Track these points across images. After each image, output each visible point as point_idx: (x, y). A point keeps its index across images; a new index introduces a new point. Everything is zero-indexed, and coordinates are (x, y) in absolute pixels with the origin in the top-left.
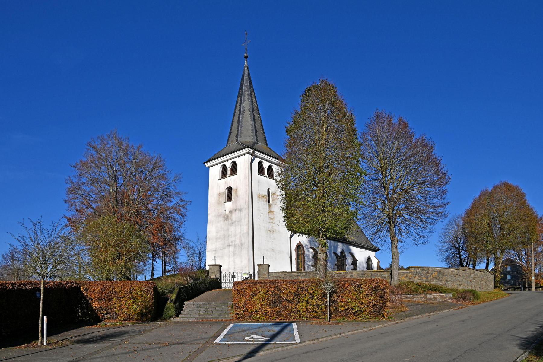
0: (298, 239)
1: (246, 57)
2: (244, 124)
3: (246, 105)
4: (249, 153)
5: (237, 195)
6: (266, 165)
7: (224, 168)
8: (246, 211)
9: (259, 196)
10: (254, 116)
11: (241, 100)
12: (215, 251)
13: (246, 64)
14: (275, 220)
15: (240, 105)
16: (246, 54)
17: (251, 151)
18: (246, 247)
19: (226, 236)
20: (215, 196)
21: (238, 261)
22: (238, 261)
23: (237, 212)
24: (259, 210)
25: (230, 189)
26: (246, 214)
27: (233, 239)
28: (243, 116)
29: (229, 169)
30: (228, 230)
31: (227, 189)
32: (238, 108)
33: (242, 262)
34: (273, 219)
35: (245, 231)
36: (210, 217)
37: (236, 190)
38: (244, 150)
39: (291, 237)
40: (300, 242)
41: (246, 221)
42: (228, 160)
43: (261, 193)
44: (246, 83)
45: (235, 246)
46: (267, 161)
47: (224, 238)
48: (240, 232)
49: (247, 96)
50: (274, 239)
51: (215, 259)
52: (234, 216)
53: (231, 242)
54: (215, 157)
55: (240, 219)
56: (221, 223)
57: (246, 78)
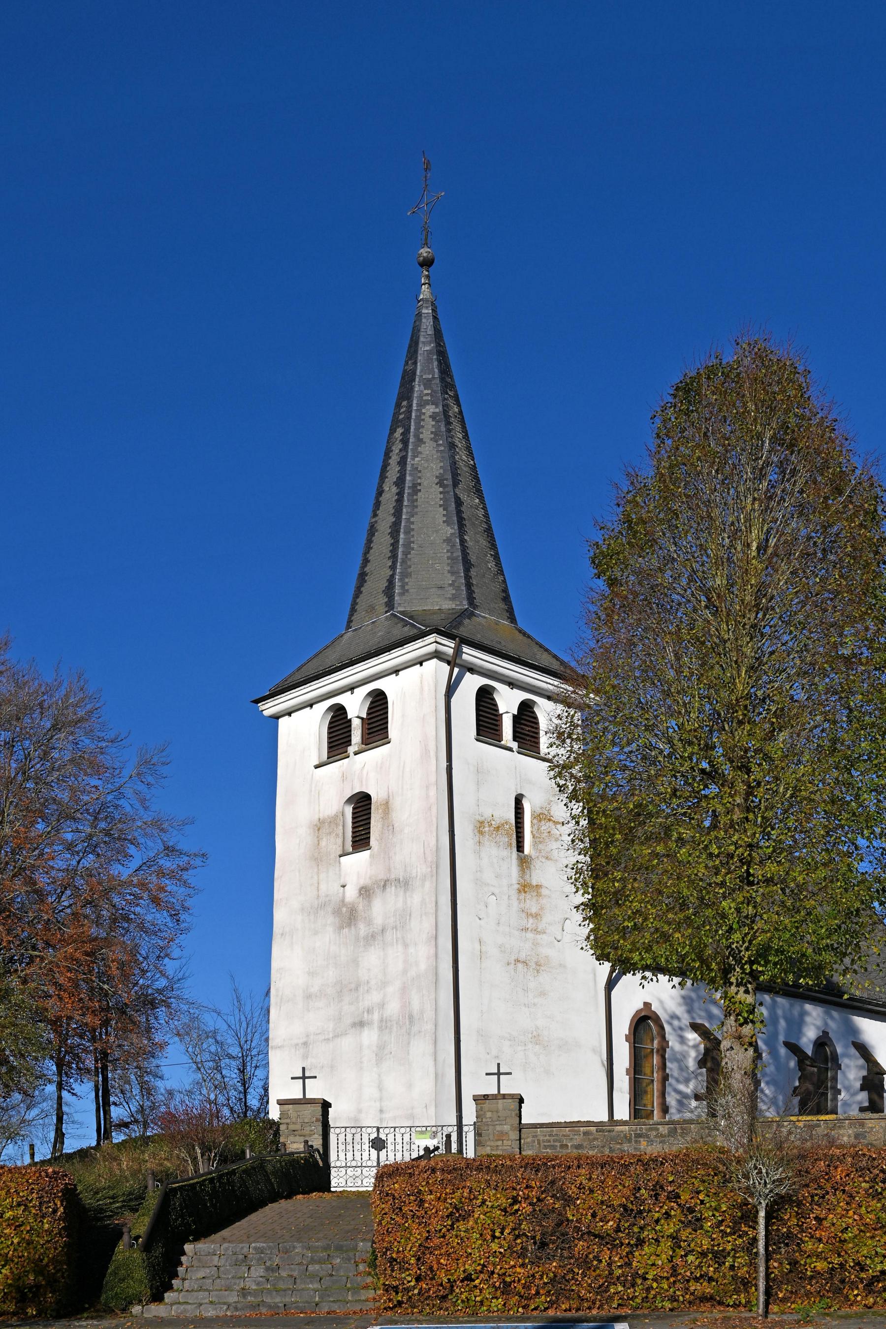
1: (427, 263)
3: (428, 460)
4: (437, 655)
5: (389, 826)
6: (508, 702)
7: (338, 720)
9: (481, 827)
10: (459, 503)
11: (405, 442)
12: (305, 1044)
13: (425, 292)
15: (403, 462)
16: (424, 252)
17: (448, 647)
18: (430, 1027)
19: (349, 988)
23: (391, 890)
24: (479, 882)
25: (362, 804)
26: (425, 902)
27: (375, 997)
29: (356, 724)
31: (349, 801)
32: (393, 473)
33: (410, 1086)
34: (536, 916)
35: (423, 966)
36: (280, 916)
39: (611, 985)
41: (427, 925)
42: (351, 688)
43: (487, 813)
44: (426, 368)
45: (384, 1025)
46: (512, 684)
47: (340, 993)
48: (405, 972)
49: (429, 424)
50: (543, 994)
51: (304, 1078)
52: (381, 909)
53: (369, 1011)
54: (298, 677)
55: (404, 918)
56: (327, 939)
57: (426, 347)
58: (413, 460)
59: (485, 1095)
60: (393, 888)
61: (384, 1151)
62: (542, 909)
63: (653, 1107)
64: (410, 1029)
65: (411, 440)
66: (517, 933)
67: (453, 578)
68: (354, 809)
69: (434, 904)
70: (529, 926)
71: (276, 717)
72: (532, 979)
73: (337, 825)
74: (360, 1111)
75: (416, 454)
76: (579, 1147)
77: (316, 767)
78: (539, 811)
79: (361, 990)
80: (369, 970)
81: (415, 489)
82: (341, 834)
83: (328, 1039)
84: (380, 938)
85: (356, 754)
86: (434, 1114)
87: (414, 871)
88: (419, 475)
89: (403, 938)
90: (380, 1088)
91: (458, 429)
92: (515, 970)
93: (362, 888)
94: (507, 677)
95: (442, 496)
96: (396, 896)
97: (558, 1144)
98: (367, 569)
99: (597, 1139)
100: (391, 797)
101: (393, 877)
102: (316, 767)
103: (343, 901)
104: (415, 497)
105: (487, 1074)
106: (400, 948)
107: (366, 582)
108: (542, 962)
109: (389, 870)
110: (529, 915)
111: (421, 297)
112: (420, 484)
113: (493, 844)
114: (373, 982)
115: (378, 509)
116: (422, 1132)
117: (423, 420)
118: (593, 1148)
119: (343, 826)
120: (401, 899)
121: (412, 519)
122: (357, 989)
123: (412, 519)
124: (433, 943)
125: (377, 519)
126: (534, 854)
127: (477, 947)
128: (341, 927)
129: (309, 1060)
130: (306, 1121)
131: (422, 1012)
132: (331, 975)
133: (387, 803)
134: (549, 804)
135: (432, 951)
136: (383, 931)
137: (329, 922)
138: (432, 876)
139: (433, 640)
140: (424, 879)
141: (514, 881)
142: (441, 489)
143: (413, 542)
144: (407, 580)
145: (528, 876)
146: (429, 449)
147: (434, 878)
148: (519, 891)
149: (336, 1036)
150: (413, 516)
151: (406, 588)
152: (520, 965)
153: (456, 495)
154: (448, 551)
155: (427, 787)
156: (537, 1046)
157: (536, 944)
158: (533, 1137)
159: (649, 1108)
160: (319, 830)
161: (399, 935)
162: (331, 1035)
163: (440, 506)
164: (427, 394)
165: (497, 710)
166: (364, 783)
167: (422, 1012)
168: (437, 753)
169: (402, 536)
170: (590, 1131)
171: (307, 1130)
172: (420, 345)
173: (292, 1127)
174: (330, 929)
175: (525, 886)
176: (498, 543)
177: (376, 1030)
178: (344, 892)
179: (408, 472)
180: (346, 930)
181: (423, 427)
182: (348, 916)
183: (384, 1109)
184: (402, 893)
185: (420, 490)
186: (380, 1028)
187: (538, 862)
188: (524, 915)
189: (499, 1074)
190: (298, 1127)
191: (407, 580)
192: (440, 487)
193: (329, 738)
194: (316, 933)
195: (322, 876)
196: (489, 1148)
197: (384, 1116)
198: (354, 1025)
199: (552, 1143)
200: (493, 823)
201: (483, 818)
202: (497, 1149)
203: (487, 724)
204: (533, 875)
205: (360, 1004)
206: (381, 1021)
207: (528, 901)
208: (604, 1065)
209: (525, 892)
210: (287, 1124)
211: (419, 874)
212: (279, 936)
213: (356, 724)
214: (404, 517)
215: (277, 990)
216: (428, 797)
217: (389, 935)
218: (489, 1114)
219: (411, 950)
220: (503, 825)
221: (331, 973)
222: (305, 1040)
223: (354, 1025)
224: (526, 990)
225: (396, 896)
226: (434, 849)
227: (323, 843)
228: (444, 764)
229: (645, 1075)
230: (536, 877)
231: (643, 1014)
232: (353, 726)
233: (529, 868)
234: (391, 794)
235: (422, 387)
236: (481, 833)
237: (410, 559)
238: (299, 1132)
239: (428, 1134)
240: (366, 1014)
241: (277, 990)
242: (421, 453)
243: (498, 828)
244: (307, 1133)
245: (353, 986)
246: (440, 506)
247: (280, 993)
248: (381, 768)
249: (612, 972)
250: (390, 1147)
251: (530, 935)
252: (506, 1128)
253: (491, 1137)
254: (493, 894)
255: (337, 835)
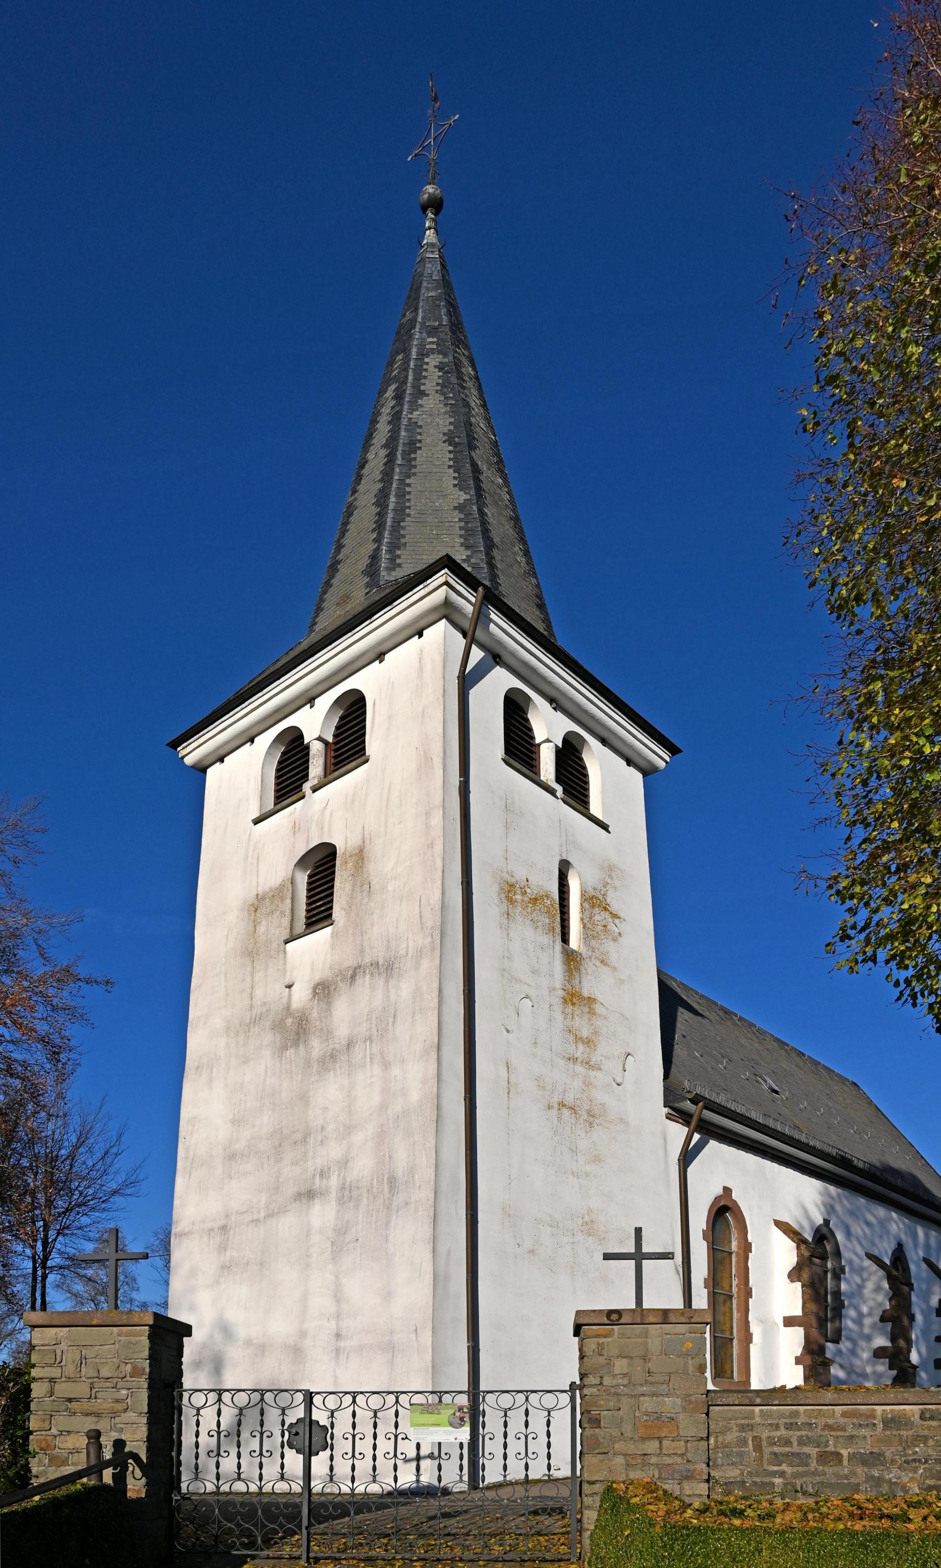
0: (724, 1168)
1: (436, 205)
2: (415, 504)
5: (364, 885)
6: (548, 727)
7: (293, 750)
8: (428, 965)
9: (510, 891)
10: (476, 470)
12: (224, 1228)
13: (430, 236)
14: (605, 1049)
17: (467, 600)
18: (426, 1194)
19: (293, 1139)
20: (234, 917)
21: (360, 1289)
22: (360, 1289)
23: (364, 981)
24: (505, 973)
25: (321, 865)
26: (418, 1002)
27: (334, 1151)
28: (409, 463)
29: (317, 749)
30: (304, 1099)
31: (302, 862)
33: (387, 1295)
34: (588, 1042)
35: (415, 1096)
36: (197, 1041)
37: (360, 856)
38: (419, 591)
39: (687, 1157)
40: (727, 1191)
41: (425, 1028)
42: (309, 699)
43: (520, 874)
45: (348, 1195)
46: (557, 702)
47: (278, 1149)
48: (383, 1107)
49: (432, 378)
50: (597, 1159)
52: (344, 1014)
53: (323, 1174)
55: (383, 1023)
56: (263, 1066)
58: (411, 413)
59: (610, 1312)
60: (368, 977)
61: (324, 1455)
62: (596, 1033)
63: (732, 1333)
64: (391, 1199)
65: (408, 392)
66: (561, 1063)
67: (469, 553)
68: (310, 877)
69: (435, 994)
70: (578, 1054)
71: (201, 769)
72: (583, 1135)
73: (282, 899)
74: (303, 1334)
75: (414, 406)
76: (871, 1459)
77: (256, 822)
78: (591, 892)
79: (311, 1141)
80: (325, 1108)
81: (413, 446)
82: (288, 912)
83: (258, 1220)
84: (344, 1058)
85: (315, 789)
86: (430, 1343)
87: (404, 946)
88: (419, 430)
89: (382, 1053)
90: (338, 1297)
91: (475, 392)
92: (559, 1118)
93: (319, 984)
94: (550, 683)
95: (452, 456)
96: (373, 988)
97: (813, 1451)
98: (340, 557)
99: (925, 1439)
100: (367, 841)
101: (367, 960)
102: (256, 822)
103: (288, 1008)
104: (413, 456)
105: (607, 1257)
106: (377, 1070)
107: (338, 571)
108: (597, 1112)
109: (362, 951)
110: (578, 1039)
111: (425, 242)
112: (420, 441)
113: (528, 922)
114: (331, 1127)
115: (359, 484)
116: (427, 1409)
117: (426, 370)
118: (910, 1463)
119: (293, 899)
120: (380, 993)
121: (408, 481)
122: (304, 1140)
123: (408, 481)
124: (434, 1056)
125: (356, 495)
126: (583, 950)
127: (503, 1072)
128: (284, 1048)
129: (228, 1254)
130: (105, 1373)
131: (412, 1170)
132: (266, 1121)
133: (361, 851)
134: (605, 887)
135: (432, 1069)
136: (349, 1045)
137: (265, 1043)
138: (433, 949)
139: (442, 580)
140: (420, 954)
141: (558, 985)
142: (451, 448)
143: (409, 507)
144: (398, 552)
145: (576, 982)
146: (432, 402)
147: (437, 952)
148: (565, 1001)
149: (269, 1216)
150: (409, 477)
151: (398, 561)
152: (566, 1112)
153: (472, 459)
154: (460, 520)
155: (427, 814)
156: (591, 1238)
157: (587, 1084)
158: (742, 1428)
159: (727, 1335)
160: (256, 911)
161: (375, 1050)
162: (262, 1214)
163: (450, 467)
164: (432, 343)
165: (533, 738)
166: (326, 829)
167: (412, 1170)
168: (444, 758)
169: (393, 499)
170: (904, 1414)
171: (104, 1401)
172: (423, 291)
173: (62, 1389)
174: (267, 1053)
175: (572, 995)
176: (528, 539)
177: (333, 1202)
178: (290, 996)
179: (403, 427)
180: (291, 1052)
181: (425, 377)
182: (294, 1029)
183: (344, 1332)
184: (381, 982)
185: (420, 448)
186: (341, 1201)
187: (590, 964)
188: (571, 1038)
189: (639, 1256)
190: (81, 1390)
191: (398, 552)
192: (450, 445)
193: (277, 784)
194: (246, 1061)
195: (259, 976)
196: (620, 1460)
197: (342, 1344)
198: (299, 1196)
199: (795, 1448)
200: (528, 891)
201: (513, 880)
202: (646, 1464)
203: (520, 748)
204: (584, 982)
205: (309, 1163)
206: (343, 1188)
207: (577, 1018)
208: (678, 1272)
209: (573, 1004)
210: (52, 1380)
211: (411, 950)
212: (193, 1071)
213: (317, 749)
214: (396, 477)
215: (187, 1150)
216: (428, 826)
217: (358, 1052)
218: (620, 1366)
219: (396, 1071)
220: (542, 897)
221: (266, 1119)
222: (223, 1222)
223: (299, 1196)
224: (574, 1151)
225: (373, 988)
226: (438, 906)
227: (262, 929)
228: (456, 780)
229: (722, 1288)
230: (588, 987)
231: (722, 1203)
232: (311, 753)
233: (578, 970)
234: (367, 836)
235: (424, 334)
236: (511, 901)
237: (404, 528)
238: (85, 1405)
239: (446, 1414)
240: (318, 1177)
241: (187, 1150)
242: (421, 406)
243: (534, 901)
244: (108, 1406)
245: (299, 1136)
246: (450, 467)
247: (191, 1154)
248: (353, 801)
249: (689, 1138)
250: (342, 1447)
251: (580, 1069)
252: (671, 1404)
253: (628, 1429)
254: (527, 997)
255: (283, 913)
